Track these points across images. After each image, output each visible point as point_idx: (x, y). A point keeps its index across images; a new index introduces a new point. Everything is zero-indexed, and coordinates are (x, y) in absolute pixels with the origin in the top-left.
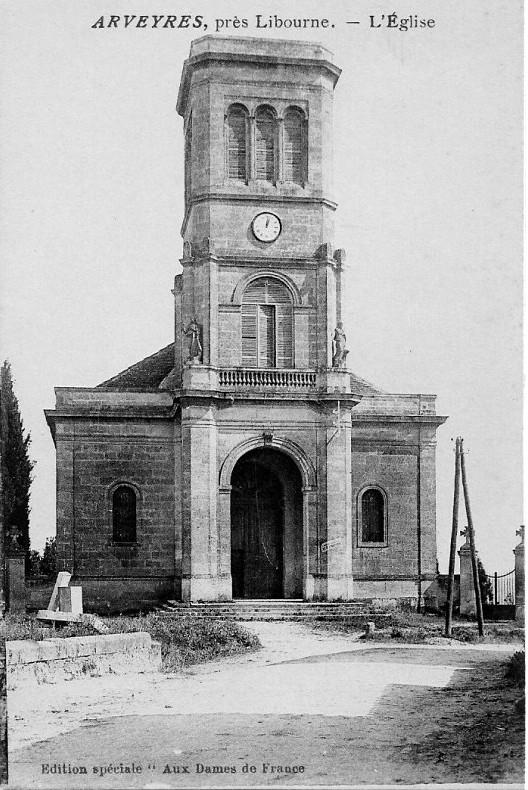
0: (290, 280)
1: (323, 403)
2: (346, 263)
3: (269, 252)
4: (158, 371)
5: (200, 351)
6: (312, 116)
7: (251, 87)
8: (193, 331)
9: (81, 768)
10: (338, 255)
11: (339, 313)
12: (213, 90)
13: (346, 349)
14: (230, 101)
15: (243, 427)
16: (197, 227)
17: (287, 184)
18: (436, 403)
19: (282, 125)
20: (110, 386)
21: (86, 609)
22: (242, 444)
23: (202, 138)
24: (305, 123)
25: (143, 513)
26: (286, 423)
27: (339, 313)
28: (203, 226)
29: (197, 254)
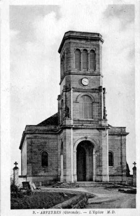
0: (92, 96)
1: (101, 128)
2: (106, 91)
3: (86, 88)
4: (53, 121)
5: (68, 115)
6: (97, 52)
7: (82, 45)
8: (64, 108)
9: (73, 212)
10: (104, 89)
11: (104, 104)
12: (71, 45)
13: (107, 114)
14: (76, 48)
15: (80, 134)
16: (67, 81)
17: (90, 70)
18: (126, 129)
19: (82, 53)
20: (40, 125)
21: (36, 186)
22: (82, 138)
23: (68, 58)
24: (95, 54)
25: (49, 159)
26: (90, 135)
27: (104, 104)
28: (68, 82)
29: (67, 89)
